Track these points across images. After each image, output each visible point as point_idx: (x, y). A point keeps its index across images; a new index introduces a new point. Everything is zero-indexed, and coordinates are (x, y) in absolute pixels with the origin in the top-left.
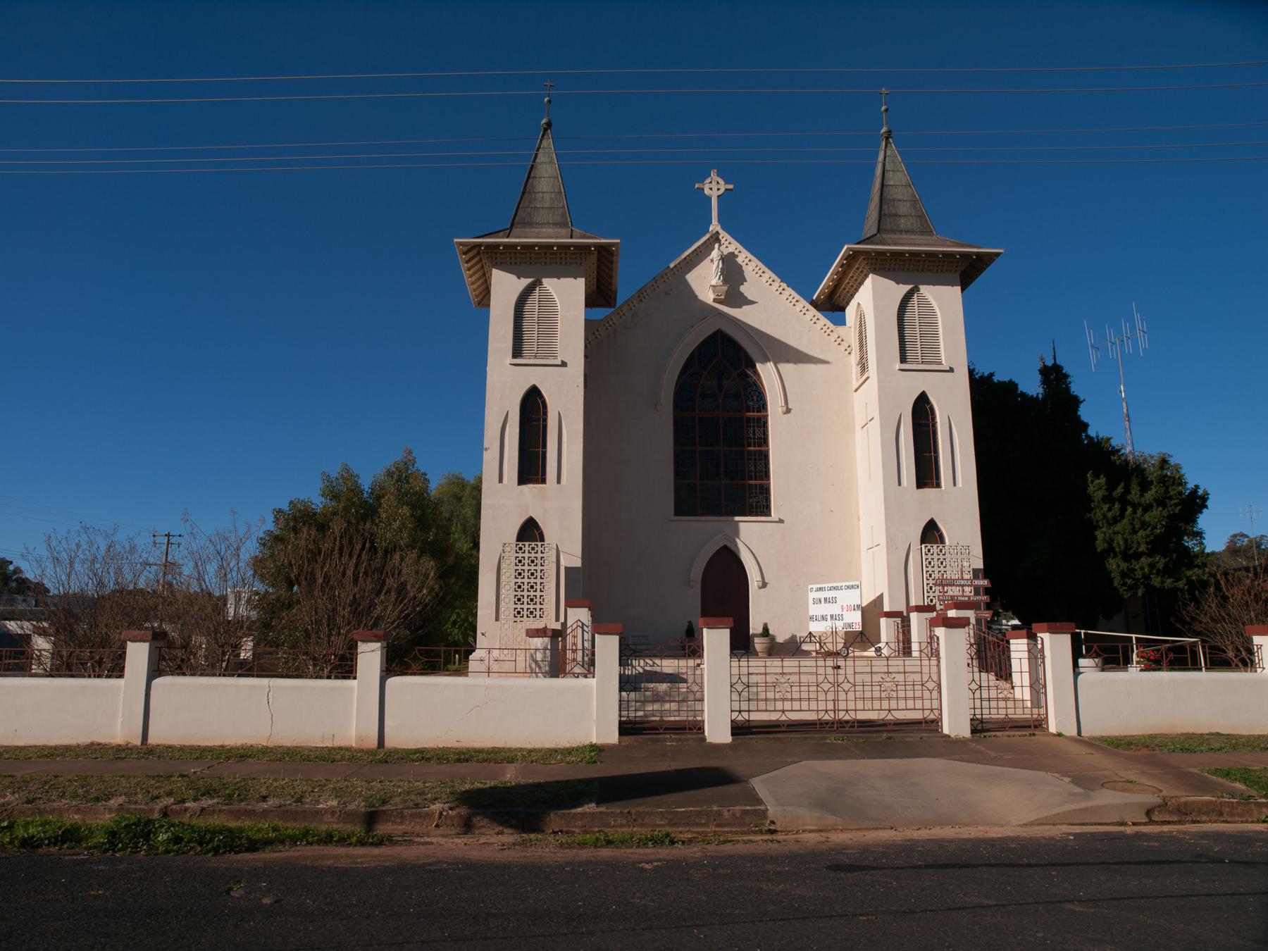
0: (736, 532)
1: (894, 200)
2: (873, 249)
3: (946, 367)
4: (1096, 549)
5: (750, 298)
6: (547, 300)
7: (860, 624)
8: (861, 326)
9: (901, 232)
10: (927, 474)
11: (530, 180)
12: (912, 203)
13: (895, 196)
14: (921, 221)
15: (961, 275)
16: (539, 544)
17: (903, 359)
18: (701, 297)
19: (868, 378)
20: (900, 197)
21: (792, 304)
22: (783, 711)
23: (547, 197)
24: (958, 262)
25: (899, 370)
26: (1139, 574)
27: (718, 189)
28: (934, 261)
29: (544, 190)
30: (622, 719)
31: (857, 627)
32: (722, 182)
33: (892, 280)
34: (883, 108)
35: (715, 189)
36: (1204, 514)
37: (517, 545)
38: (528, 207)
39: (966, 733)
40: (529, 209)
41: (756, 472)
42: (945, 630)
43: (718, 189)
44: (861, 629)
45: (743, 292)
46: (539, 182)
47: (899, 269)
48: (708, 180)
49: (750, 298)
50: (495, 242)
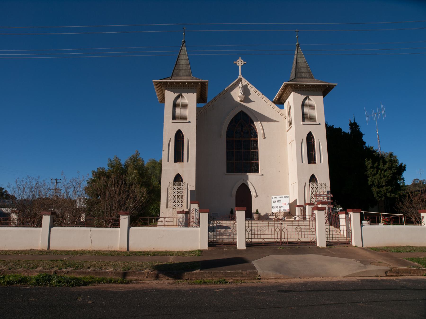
0: (247, 179)
1: (300, 67)
2: (293, 83)
3: (318, 123)
4: (368, 184)
5: (252, 100)
6: (184, 101)
7: (289, 209)
9: (303, 78)
10: (311, 159)
11: (178, 61)
12: (306, 68)
13: (301, 66)
14: (309, 74)
15: (323, 92)
16: (181, 182)
17: (303, 121)
18: (235, 100)
19: (292, 127)
20: (302, 66)
21: (266, 102)
22: (263, 239)
23: (184, 66)
24: (322, 88)
25: (302, 124)
29: (183, 64)
30: (209, 241)
31: (288, 210)
32: (242, 61)
33: (300, 94)
34: (297, 36)
35: (240, 63)
36: (404, 172)
37: (174, 183)
38: (178, 70)
39: (325, 246)
40: (178, 70)
42: (318, 211)
43: (241, 64)
44: (289, 211)
45: (250, 98)
46: (181, 61)
47: (302, 90)
48: (238, 60)
49: (252, 100)
50: (166, 81)
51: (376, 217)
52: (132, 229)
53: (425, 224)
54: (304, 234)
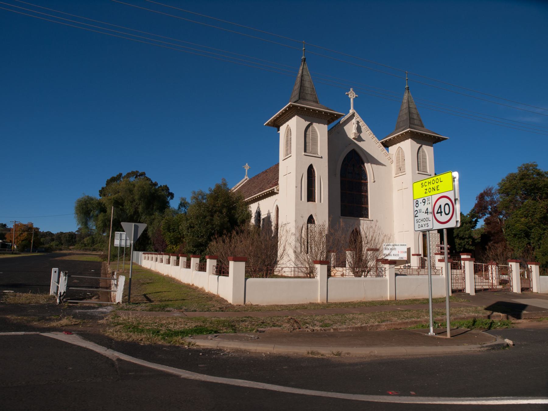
0: (359, 224)
3: (319, 155)
4: (453, 235)
5: (363, 139)
6: (314, 131)
7: (407, 258)
8: (287, 136)
9: (415, 125)
10: (311, 197)
11: (302, 81)
16: (313, 225)
17: (305, 151)
18: (349, 136)
19: (291, 156)
21: (376, 143)
22: (482, 286)
24: (299, 110)
25: (304, 155)
26: (463, 244)
27: (353, 96)
30: (477, 287)
31: (405, 258)
32: (354, 94)
33: (416, 142)
34: (304, 48)
35: (352, 96)
36: (477, 226)
39: (519, 292)
40: (304, 93)
42: (516, 264)
44: (407, 259)
45: (361, 136)
47: (312, 116)
49: (363, 139)
53: (386, 276)
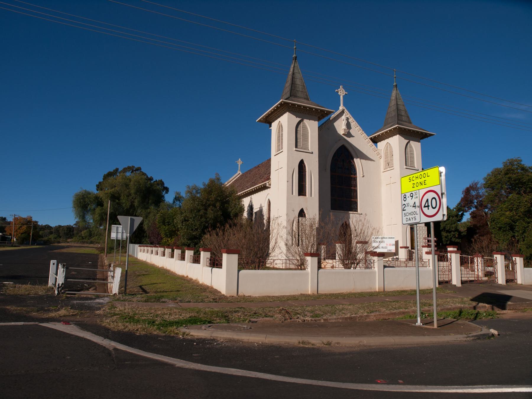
0: (348, 218)
3: (310, 151)
4: (440, 228)
5: (353, 135)
6: (305, 127)
7: (395, 250)
9: (403, 121)
10: (302, 191)
11: (293, 79)
16: (304, 218)
17: (296, 147)
18: (338, 132)
19: (282, 151)
21: (365, 139)
22: (468, 278)
24: (291, 107)
25: (295, 150)
26: (449, 237)
27: (343, 93)
28: (294, 107)
30: (463, 279)
32: (344, 91)
33: (404, 138)
34: (295, 47)
35: (342, 93)
36: (463, 219)
39: (504, 283)
40: (295, 91)
41: (353, 196)
42: (501, 256)
44: (395, 252)
45: (351, 132)
47: (302, 113)
49: (352, 135)
51: (469, 257)
52: (243, 272)
54: (445, 275)
